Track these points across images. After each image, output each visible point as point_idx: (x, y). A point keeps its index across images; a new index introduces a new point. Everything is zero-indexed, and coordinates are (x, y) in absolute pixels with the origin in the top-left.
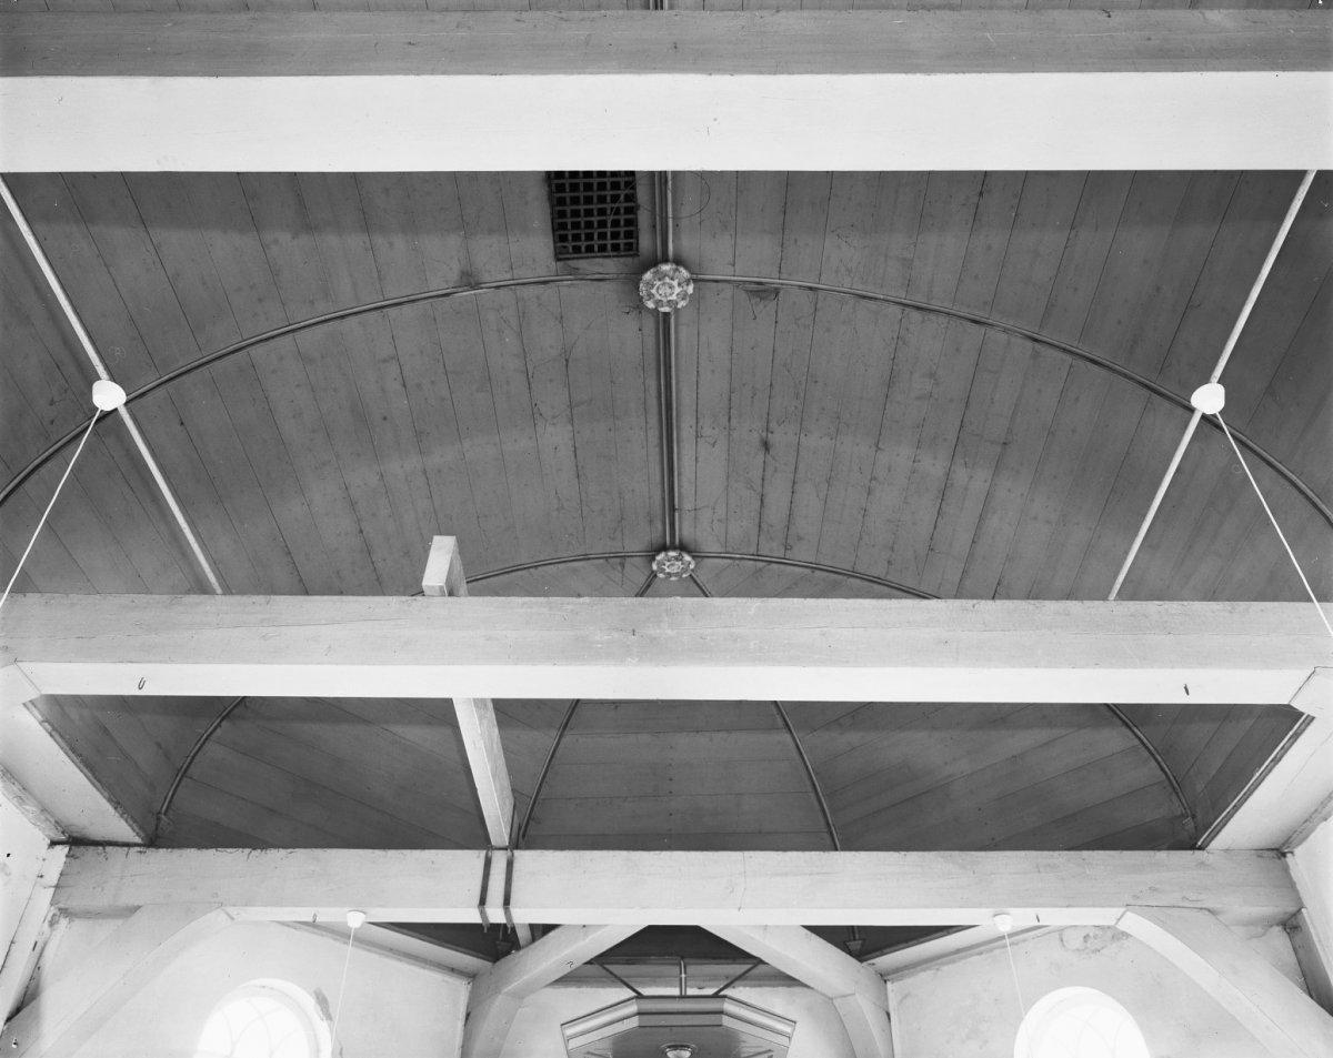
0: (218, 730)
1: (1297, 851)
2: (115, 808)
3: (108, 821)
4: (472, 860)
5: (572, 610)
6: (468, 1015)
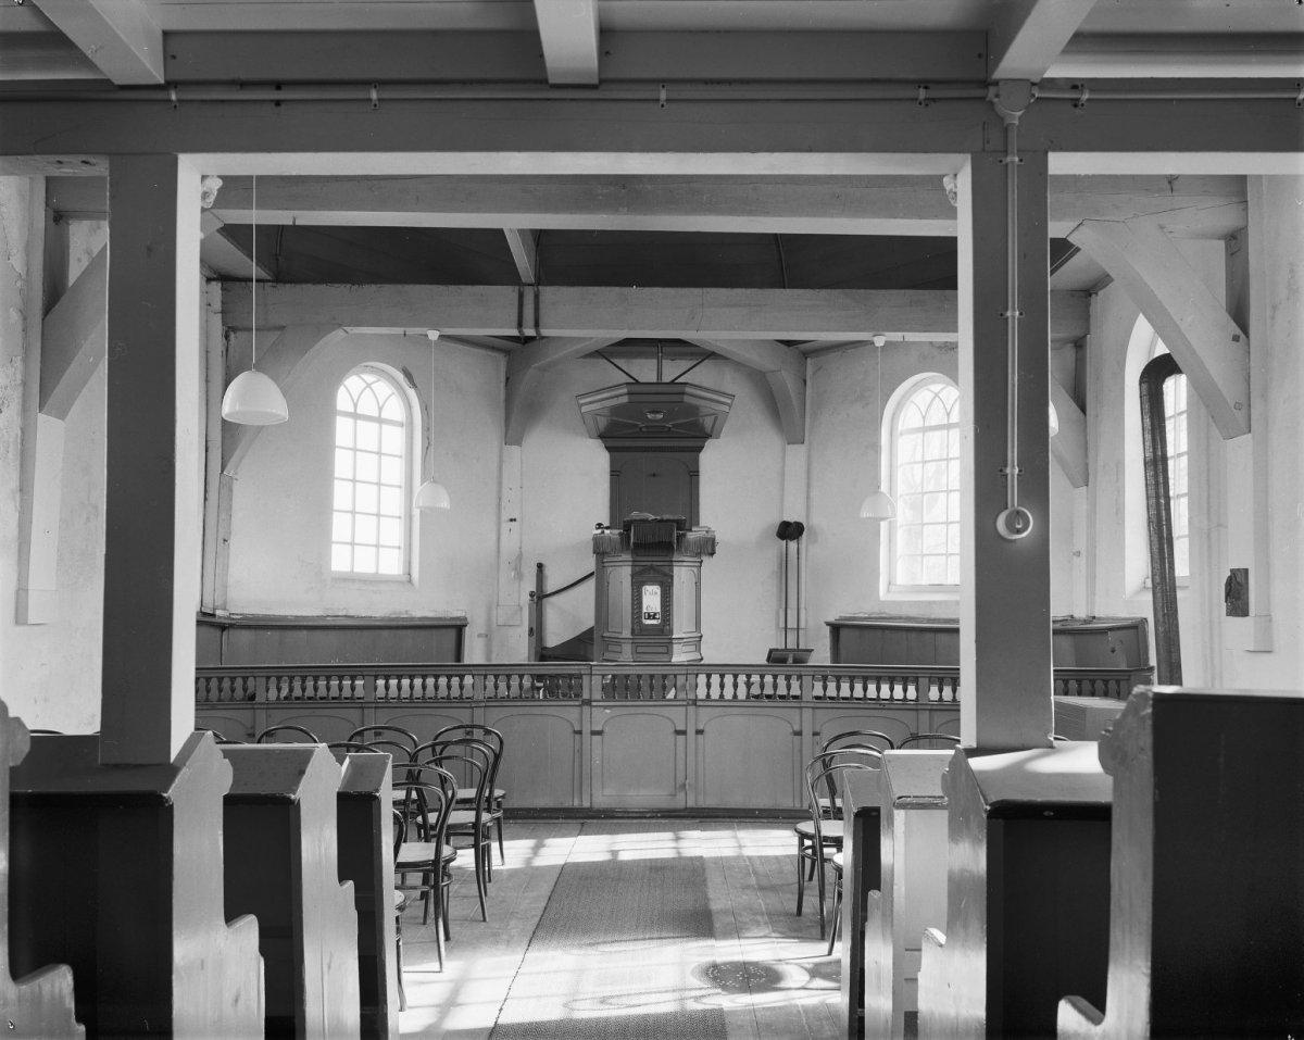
1: (1101, 293)
4: (508, 293)
6: (507, 379)
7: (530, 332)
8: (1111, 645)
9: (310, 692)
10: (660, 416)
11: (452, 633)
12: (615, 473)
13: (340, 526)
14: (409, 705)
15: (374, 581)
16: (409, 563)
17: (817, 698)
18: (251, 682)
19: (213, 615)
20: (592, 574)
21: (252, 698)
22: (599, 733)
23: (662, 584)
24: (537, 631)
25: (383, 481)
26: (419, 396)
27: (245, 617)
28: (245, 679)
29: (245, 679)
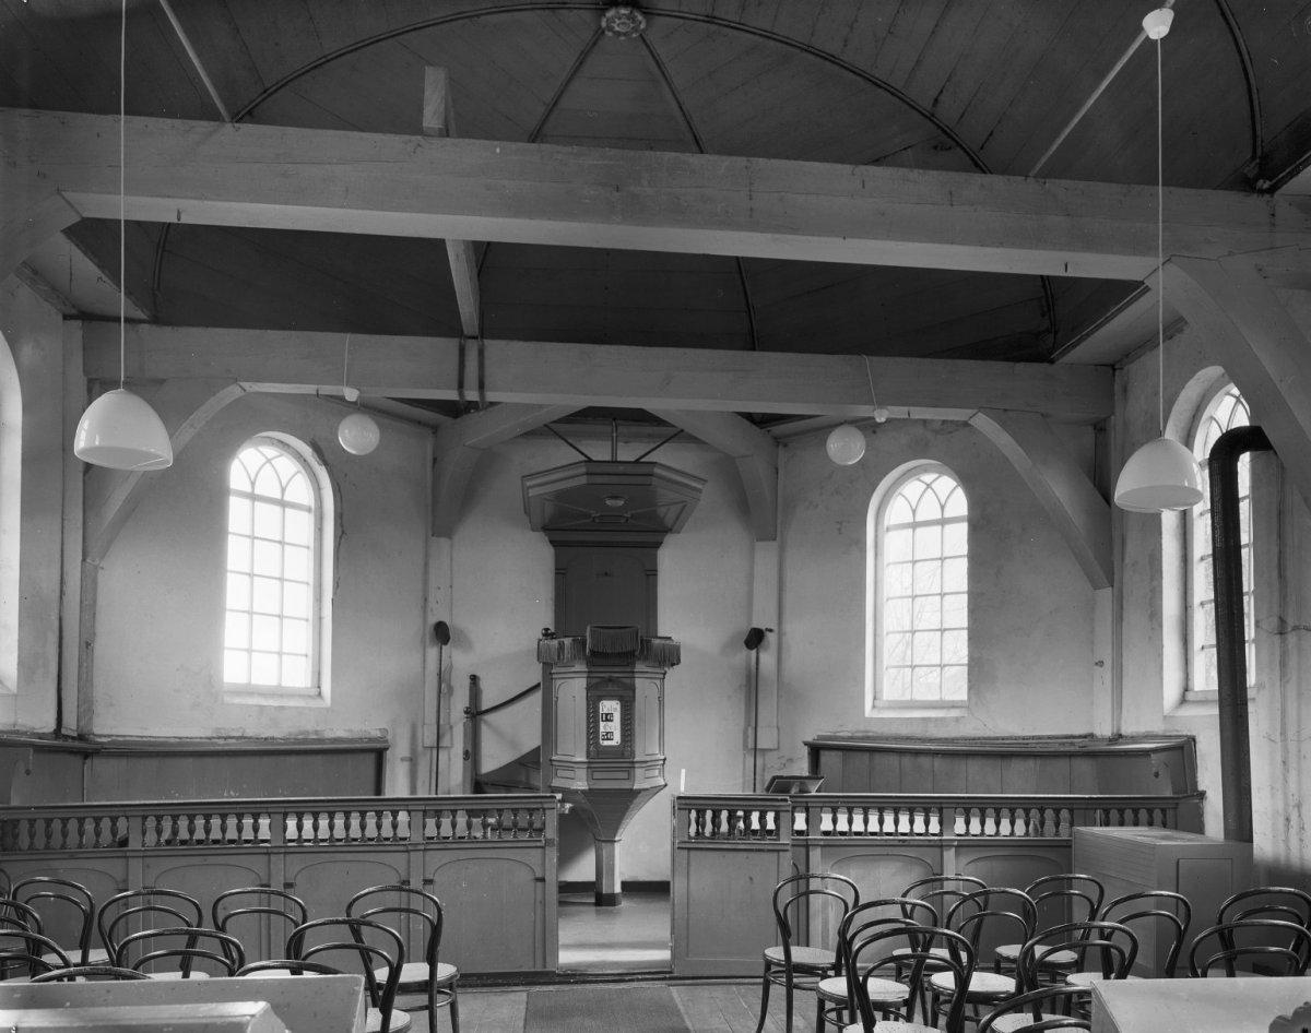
5: (561, 161)
6: (435, 460)
7: (472, 395)
8: (1154, 770)
9: (200, 834)
10: (621, 503)
11: (371, 759)
12: (561, 572)
14: (297, 850)
16: (318, 675)
17: (826, 833)
18: (122, 824)
20: (539, 685)
21: (124, 843)
23: (621, 699)
24: (472, 755)
25: (276, 656)
28: (114, 820)
29: (114, 820)
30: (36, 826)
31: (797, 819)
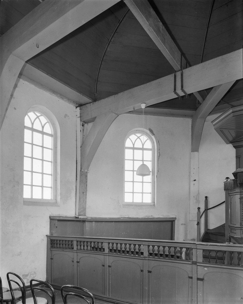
0: (102, 65)
2: (80, 94)
3: (85, 99)
11: (170, 224)
13: (128, 187)
15: (141, 206)
19: (78, 218)
20: (224, 202)
22: (202, 280)
26: (156, 138)
27: (92, 218)
30: (131, 246)
31: (115, 248)
